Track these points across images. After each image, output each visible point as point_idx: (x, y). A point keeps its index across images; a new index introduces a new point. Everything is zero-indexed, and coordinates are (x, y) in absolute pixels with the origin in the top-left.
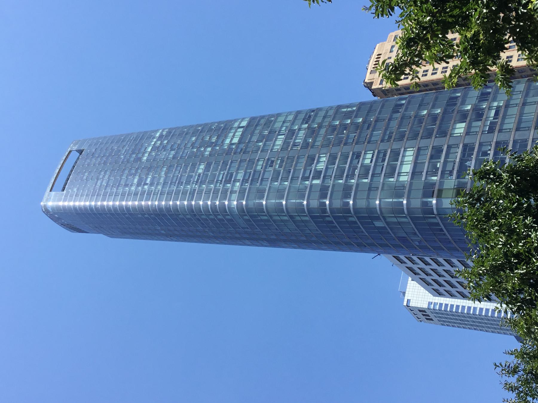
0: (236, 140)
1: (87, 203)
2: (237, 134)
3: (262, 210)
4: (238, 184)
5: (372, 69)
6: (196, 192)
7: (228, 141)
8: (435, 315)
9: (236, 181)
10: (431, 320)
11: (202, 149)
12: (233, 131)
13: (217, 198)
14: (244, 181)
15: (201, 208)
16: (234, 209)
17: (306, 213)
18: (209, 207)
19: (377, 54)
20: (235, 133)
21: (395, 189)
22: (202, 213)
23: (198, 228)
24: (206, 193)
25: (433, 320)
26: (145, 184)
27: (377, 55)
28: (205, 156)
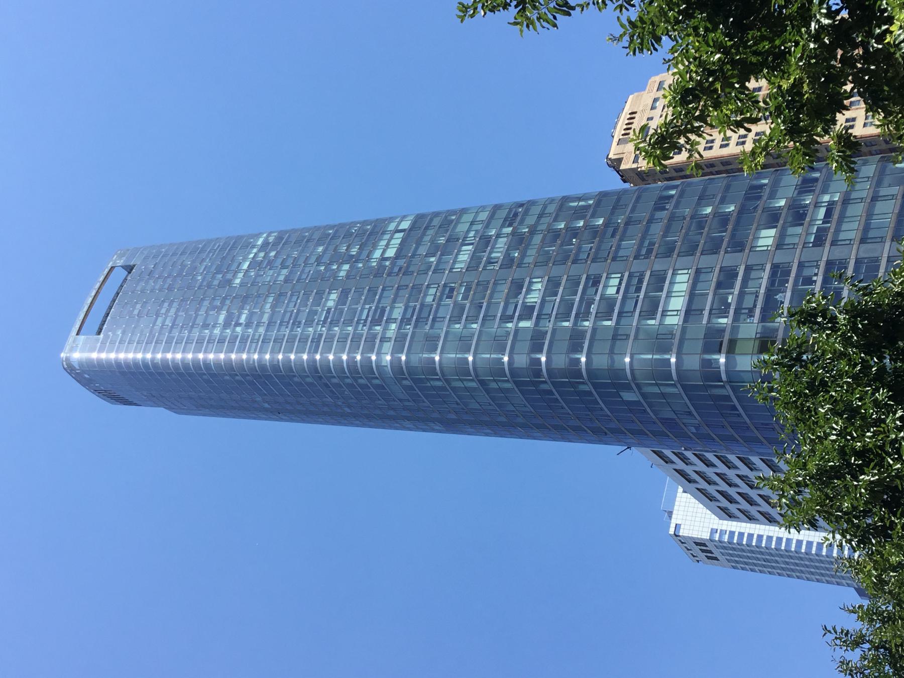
0: (391, 253)
3: (433, 371)
4: (393, 326)
5: (621, 137)
7: (377, 254)
8: (728, 558)
9: (389, 321)
10: (716, 559)
11: (335, 267)
12: (387, 237)
14: (405, 321)
16: (385, 368)
19: (630, 112)
21: (657, 339)
25: (718, 560)
27: (630, 114)
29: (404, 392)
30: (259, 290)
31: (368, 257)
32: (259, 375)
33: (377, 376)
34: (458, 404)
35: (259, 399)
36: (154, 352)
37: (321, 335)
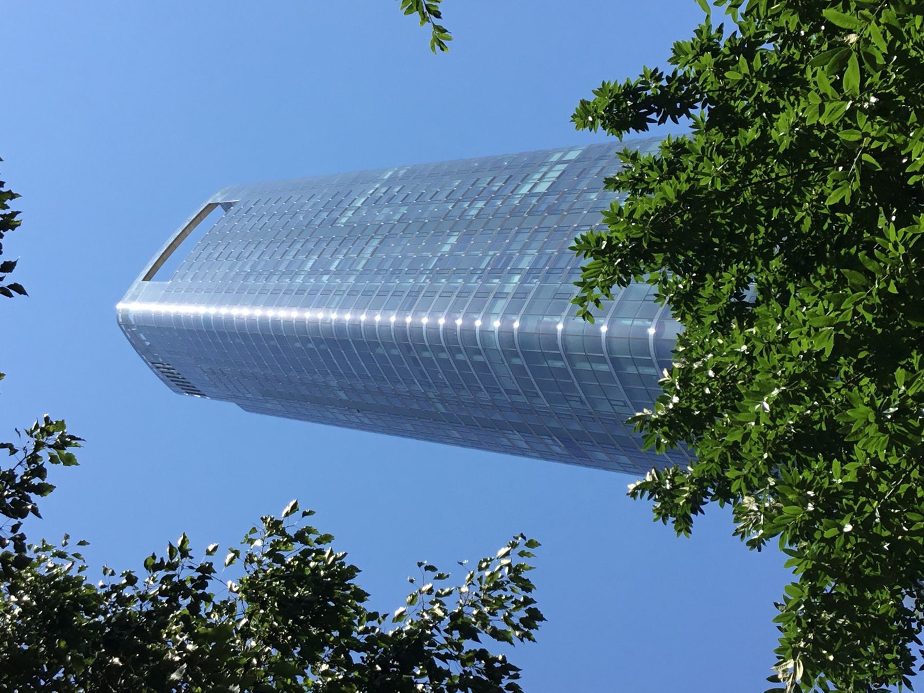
0: (542, 188)
1: (348, 317)
2: (551, 174)
3: (597, 347)
4: (516, 278)
6: (423, 292)
7: (525, 190)
9: (513, 272)
11: (466, 205)
12: (545, 169)
13: (563, 310)
14: (532, 272)
15: (393, 334)
16: (492, 335)
17: (650, 356)
18: (377, 330)
20: (546, 173)
21: (644, 300)
22: (424, 342)
23: (497, 397)
24: (336, 293)
26: (327, 272)
28: (468, 218)
29: (513, 378)
30: (521, 224)
31: (512, 192)
32: (334, 339)
33: (480, 347)
34: (582, 402)
35: (334, 383)
36: (487, 316)
37: (422, 288)
